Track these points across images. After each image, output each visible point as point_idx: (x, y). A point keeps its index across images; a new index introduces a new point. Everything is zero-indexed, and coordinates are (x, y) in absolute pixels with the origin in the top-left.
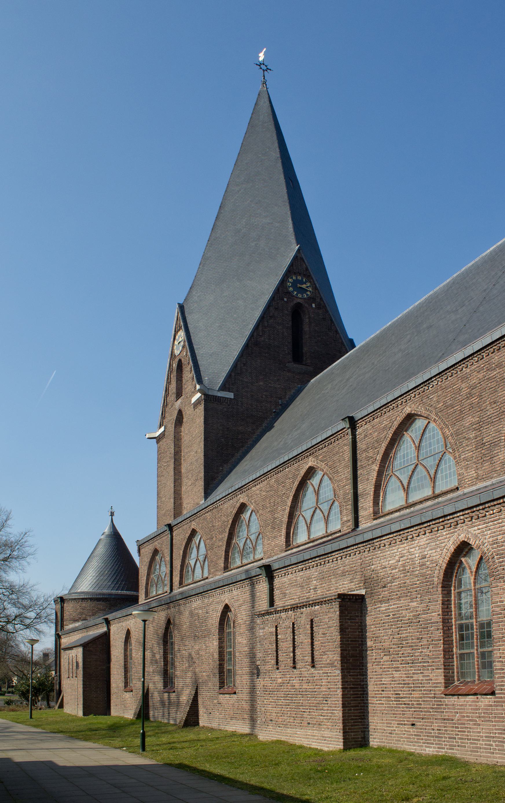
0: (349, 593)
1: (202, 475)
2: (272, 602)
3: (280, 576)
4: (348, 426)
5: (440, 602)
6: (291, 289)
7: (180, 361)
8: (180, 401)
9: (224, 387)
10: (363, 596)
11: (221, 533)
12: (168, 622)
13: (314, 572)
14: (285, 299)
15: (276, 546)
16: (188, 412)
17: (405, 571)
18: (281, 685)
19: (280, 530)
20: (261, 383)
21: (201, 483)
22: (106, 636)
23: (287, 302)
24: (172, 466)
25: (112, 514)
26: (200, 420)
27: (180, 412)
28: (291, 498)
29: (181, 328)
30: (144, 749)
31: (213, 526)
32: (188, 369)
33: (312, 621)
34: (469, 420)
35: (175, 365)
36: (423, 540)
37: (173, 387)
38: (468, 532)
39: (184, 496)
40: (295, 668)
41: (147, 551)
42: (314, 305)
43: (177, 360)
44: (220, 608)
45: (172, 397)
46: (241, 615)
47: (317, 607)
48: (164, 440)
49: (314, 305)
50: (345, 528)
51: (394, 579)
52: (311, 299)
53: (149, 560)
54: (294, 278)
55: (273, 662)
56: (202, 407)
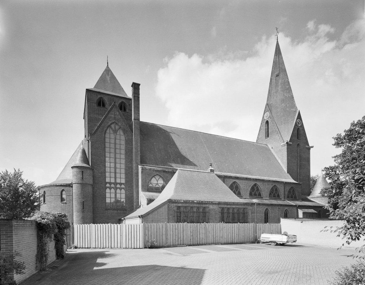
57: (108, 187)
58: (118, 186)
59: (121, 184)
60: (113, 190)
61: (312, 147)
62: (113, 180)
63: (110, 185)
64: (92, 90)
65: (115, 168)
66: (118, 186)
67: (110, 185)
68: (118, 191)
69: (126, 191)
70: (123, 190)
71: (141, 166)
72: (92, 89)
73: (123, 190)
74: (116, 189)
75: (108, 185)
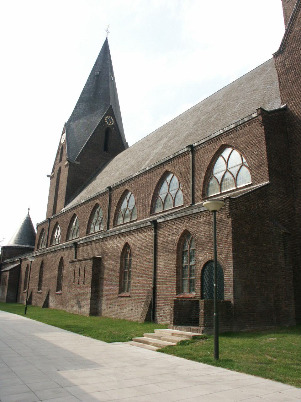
0: (98, 257)
1: (65, 196)
2: (76, 258)
3: (150, 229)
4: (109, 190)
5: (120, 263)
6: (106, 121)
7: (63, 146)
8: (61, 163)
9: (77, 160)
10: (101, 258)
11: (66, 225)
12: (42, 262)
13: (88, 247)
14: (104, 125)
15: (83, 233)
16: (63, 168)
17: (112, 250)
18: (75, 290)
19: (85, 227)
20: (91, 159)
21: (64, 200)
22: (20, 266)
23: (104, 126)
24: (55, 190)
25: (29, 209)
26: (67, 173)
27: (60, 168)
28: (90, 214)
29: (65, 133)
30: (25, 313)
31: (64, 221)
32: (22, 287)
33: (85, 266)
34: (142, 195)
35: (61, 148)
36: (117, 240)
37: (59, 156)
38: (128, 239)
39: (58, 204)
40: (79, 284)
41: (40, 228)
42: (114, 129)
43: (62, 145)
44: (60, 258)
45: (58, 161)
46: (66, 262)
47: (87, 261)
48: (53, 179)
49: (114, 129)
50: (105, 229)
51: (109, 253)
52: (113, 126)
53: (40, 233)
54: (108, 117)
55: (73, 281)
56: (68, 167)
65: (239, 125)
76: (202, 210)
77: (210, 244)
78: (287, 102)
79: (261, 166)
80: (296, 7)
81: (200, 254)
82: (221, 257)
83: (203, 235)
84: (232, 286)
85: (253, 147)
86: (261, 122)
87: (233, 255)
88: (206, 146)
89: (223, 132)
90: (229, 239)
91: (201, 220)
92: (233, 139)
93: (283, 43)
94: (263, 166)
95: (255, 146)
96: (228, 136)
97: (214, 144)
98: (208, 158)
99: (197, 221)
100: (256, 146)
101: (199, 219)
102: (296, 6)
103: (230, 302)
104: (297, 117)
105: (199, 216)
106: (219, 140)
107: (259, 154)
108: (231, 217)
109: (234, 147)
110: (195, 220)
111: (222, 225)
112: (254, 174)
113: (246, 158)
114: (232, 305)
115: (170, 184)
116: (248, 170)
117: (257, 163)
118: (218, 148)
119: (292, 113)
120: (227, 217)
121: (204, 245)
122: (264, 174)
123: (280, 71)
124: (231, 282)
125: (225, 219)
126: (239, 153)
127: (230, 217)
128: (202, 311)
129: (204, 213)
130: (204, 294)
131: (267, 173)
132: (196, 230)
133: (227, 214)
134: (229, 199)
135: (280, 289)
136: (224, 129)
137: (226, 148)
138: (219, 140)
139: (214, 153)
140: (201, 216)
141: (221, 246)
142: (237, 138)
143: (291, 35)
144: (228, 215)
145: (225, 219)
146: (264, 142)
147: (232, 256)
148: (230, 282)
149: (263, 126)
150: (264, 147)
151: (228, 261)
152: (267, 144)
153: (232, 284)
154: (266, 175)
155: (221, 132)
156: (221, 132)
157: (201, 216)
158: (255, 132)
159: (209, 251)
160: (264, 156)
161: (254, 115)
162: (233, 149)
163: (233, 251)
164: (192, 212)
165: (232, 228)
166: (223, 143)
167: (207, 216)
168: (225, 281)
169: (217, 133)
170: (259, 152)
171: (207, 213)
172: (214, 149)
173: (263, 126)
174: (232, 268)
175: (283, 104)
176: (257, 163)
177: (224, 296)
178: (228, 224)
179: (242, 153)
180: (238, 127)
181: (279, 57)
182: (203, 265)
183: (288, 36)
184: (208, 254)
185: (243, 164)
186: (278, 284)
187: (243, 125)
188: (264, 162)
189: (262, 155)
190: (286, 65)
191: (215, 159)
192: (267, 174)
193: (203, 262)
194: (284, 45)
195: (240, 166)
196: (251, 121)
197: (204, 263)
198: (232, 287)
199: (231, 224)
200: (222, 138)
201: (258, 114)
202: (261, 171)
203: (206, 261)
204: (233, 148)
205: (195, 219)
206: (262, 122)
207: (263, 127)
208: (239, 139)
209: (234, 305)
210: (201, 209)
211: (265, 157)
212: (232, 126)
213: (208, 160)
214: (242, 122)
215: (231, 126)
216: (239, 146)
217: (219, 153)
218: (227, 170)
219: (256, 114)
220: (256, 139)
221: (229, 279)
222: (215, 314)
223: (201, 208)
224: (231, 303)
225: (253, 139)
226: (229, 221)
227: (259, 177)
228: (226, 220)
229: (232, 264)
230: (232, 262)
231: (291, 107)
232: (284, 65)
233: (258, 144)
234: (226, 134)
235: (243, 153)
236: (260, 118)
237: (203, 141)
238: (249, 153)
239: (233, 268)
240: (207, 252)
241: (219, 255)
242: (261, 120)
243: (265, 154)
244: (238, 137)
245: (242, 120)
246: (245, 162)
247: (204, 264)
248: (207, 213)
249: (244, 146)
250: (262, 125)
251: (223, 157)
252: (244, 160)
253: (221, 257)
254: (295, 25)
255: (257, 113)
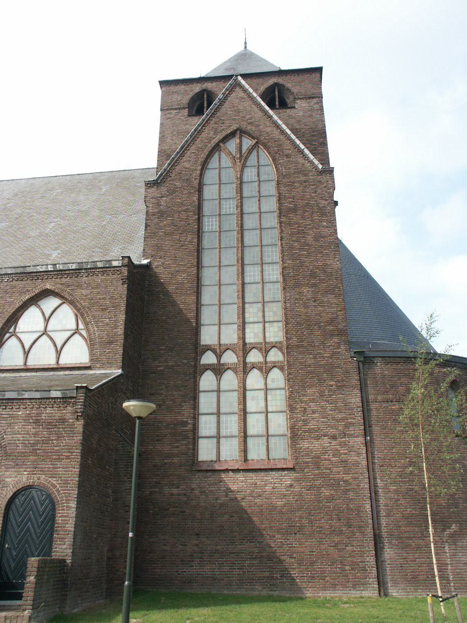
57: (207, 367)
58: (229, 358)
59: (265, 348)
60: (230, 380)
61: (250, 123)
62: (230, 336)
63: (219, 357)
64: (208, 76)
65: (86, 269)
66: (254, 357)
67: (219, 357)
68: (254, 379)
69: (290, 379)
70: (276, 374)
71: (142, 261)
72: (208, 74)
73: (276, 374)
74: (245, 369)
75: (209, 358)
76: (27, 397)
77: (34, 458)
78: (152, 257)
79: (111, 343)
80: (190, 138)
81: (8, 473)
82: (54, 482)
83: (18, 440)
84: (72, 533)
85: (103, 310)
86: (125, 278)
87: (79, 481)
88: (12, 281)
89: (52, 269)
90: (75, 454)
91: (20, 413)
92: (69, 286)
93: (163, 173)
94: (114, 343)
95: (105, 309)
96: (60, 278)
97: (29, 282)
98: (12, 302)
99: (11, 413)
100: (108, 311)
101: (14, 409)
102: (190, 135)
103: (64, 561)
104: (162, 284)
105: (16, 404)
106: (42, 279)
107: (112, 324)
108: (83, 419)
109: (66, 299)
110: (4, 410)
111: (63, 428)
112: (98, 352)
113: (86, 324)
114: (68, 566)
115: (29, 352)
116: (84, 343)
117: (105, 337)
118: (37, 291)
119: (156, 276)
120: (76, 418)
121: (19, 458)
122: (113, 357)
123: (151, 211)
124: (70, 526)
125: (71, 421)
126: (74, 312)
127: (82, 418)
128: (32, 579)
129: (27, 401)
130: (7, 546)
131: (119, 357)
132: (5, 428)
133: (77, 412)
134: (84, 390)
135: (119, 539)
136: (56, 265)
137: (50, 295)
138: (42, 279)
139: (27, 298)
140: (19, 405)
141: (57, 465)
142: (76, 288)
143: (177, 168)
144: (80, 414)
145: (71, 421)
146: (123, 307)
147: (77, 483)
148: (67, 526)
149: (127, 285)
150: (122, 317)
151: (69, 490)
152: (126, 314)
153: (73, 529)
154: (117, 359)
155: (50, 268)
156: (50, 269)
157: (21, 407)
158: (111, 289)
159: (28, 470)
160: (119, 330)
161: (115, 264)
162: (64, 303)
163: (80, 476)
164: (4, 395)
165: (83, 436)
166: (48, 286)
167: (33, 408)
168: (58, 523)
169: (42, 268)
170: (111, 322)
171: (34, 404)
172: (28, 291)
173: (127, 285)
174: (76, 503)
175: (145, 257)
176: (105, 337)
177: (52, 551)
178: (75, 429)
179: (80, 313)
180: (83, 271)
181: (153, 189)
182: (12, 494)
183: (172, 167)
184: (27, 474)
185: (77, 331)
186: (117, 532)
187: (92, 270)
188: (118, 339)
189: (116, 327)
190: (161, 205)
191: (25, 309)
192: (119, 358)
193: (13, 487)
194: (164, 176)
195: (72, 332)
196: (107, 269)
197: (15, 490)
198: (71, 536)
199: (82, 430)
200: (47, 279)
201: (122, 263)
202: (110, 350)
203: (20, 486)
204: (64, 301)
205: (5, 409)
206: (126, 277)
207: (126, 286)
208: (79, 291)
209: (72, 566)
210: (24, 395)
211: (120, 330)
212: (72, 266)
213: (12, 307)
214: (93, 267)
215: (71, 265)
216: (78, 302)
217: (34, 300)
218: (45, 332)
219: (119, 263)
220: (109, 300)
221: (66, 522)
222: (126, 583)
223: (24, 392)
224: (65, 562)
225: (104, 298)
226: (79, 425)
227: (104, 360)
228: (73, 422)
229: (76, 496)
230: (76, 492)
231: (157, 267)
232: (159, 204)
233: (112, 308)
234: (58, 274)
235: (82, 315)
236: (125, 272)
237: (9, 271)
238: (93, 316)
239: (77, 504)
240: (25, 471)
241: (50, 479)
242: (126, 275)
243: (122, 327)
244: (79, 286)
245: (93, 263)
246: (81, 329)
247: (14, 491)
248: (34, 404)
249: (87, 304)
250: (125, 282)
251: (41, 309)
252: (81, 326)
253: (54, 482)
254: (184, 159)
255: (121, 262)
